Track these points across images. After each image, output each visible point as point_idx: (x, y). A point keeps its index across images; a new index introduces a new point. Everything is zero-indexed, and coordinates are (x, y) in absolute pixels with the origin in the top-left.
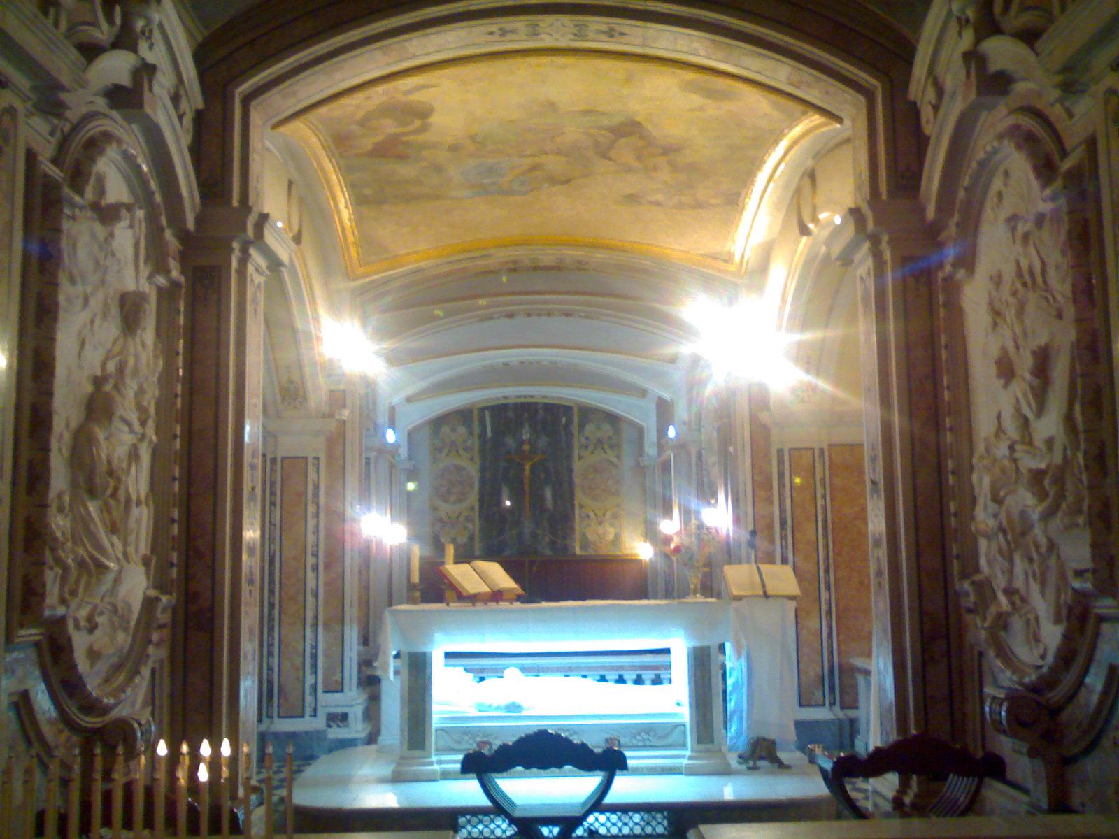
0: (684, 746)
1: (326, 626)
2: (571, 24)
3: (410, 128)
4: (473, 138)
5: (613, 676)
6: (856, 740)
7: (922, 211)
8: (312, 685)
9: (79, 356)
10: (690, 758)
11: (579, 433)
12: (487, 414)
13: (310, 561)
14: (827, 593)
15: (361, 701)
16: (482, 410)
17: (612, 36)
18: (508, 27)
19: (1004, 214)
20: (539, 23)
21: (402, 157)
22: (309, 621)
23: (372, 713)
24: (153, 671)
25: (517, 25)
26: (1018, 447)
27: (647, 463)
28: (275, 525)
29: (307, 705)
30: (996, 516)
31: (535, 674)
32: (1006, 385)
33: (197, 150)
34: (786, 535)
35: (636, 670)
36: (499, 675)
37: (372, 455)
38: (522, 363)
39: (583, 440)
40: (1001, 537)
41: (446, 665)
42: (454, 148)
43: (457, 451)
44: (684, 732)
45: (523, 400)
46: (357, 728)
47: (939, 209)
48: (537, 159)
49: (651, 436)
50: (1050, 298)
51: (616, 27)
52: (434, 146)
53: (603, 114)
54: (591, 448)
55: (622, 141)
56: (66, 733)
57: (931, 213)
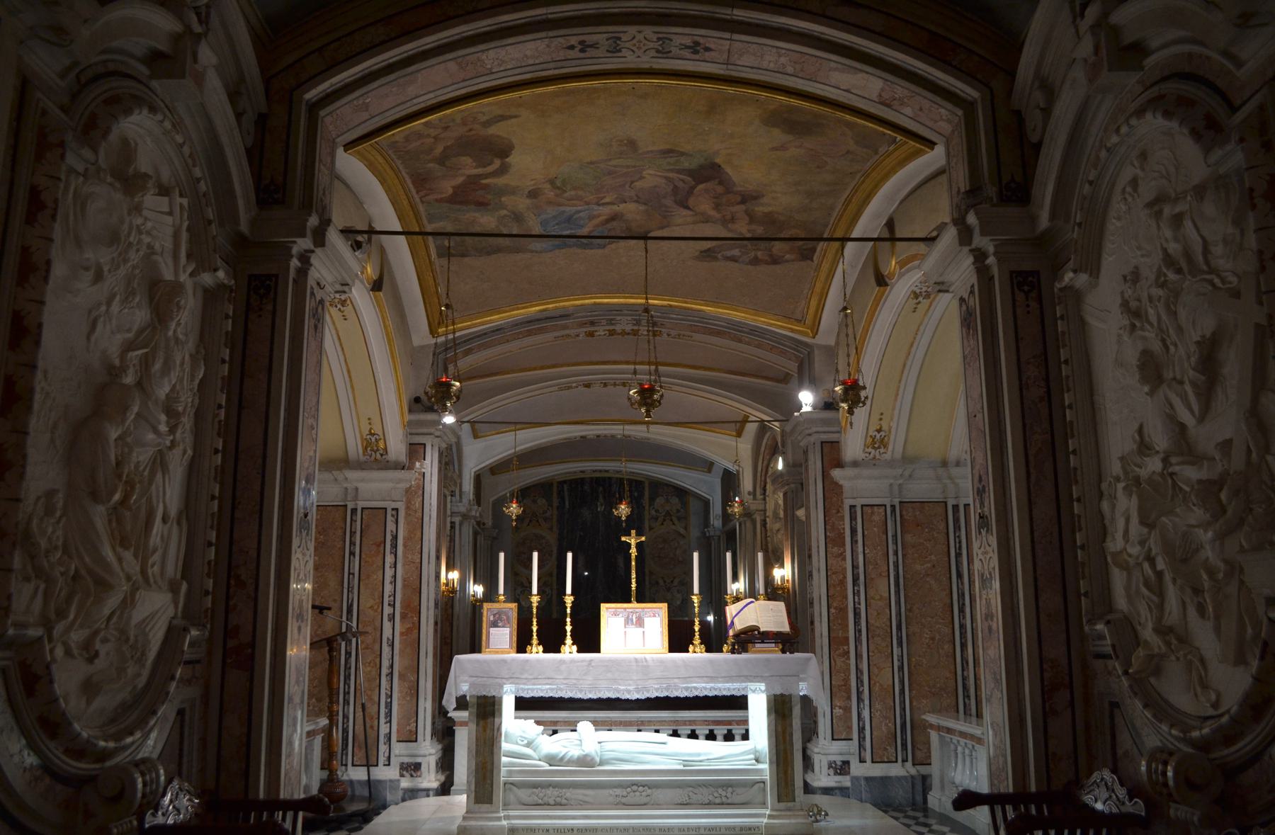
0: (764, 805)
1: (401, 676)
2: (655, 38)
3: (490, 169)
4: (552, 182)
5: (686, 730)
6: (929, 797)
7: (1034, 219)
8: (386, 734)
9: (88, 338)
10: (770, 817)
11: (650, 506)
12: (566, 487)
13: (387, 610)
14: (860, 667)
15: (433, 751)
16: (562, 483)
17: (696, 52)
18: (590, 39)
19: (1148, 190)
20: (621, 35)
21: (482, 205)
22: (385, 671)
23: (446, 763)
24: (181, 713)
25: (595, 38)
26: (1173, 460)
27: (712, 533)
28: (353, 574)
29: (381, 754)
30: (1142, 543)
31: (608, 728)
32: (1151, 393)
33: (255, 155)
34: (859, 591)
35: (708, 725)
36: (572, 728)
37: (457, 520)
38: (598, 436)
39: (653, 512)
40: (1146, 566)
41: (516, 718)
42: (533, 194)
43: (538, 521)
44: (764, 790)
45: (598, 475)
46: (430, 779)
47: (1053, 216)
48: (615, 208)
49: (716, 509)
50: (1217, 281)
51: (702, 40)
52: (513, 191)
53: (682, 154)
54: (660, 519)
55: (701, 186)
56: (47, 780)
57: (1044, 222)
